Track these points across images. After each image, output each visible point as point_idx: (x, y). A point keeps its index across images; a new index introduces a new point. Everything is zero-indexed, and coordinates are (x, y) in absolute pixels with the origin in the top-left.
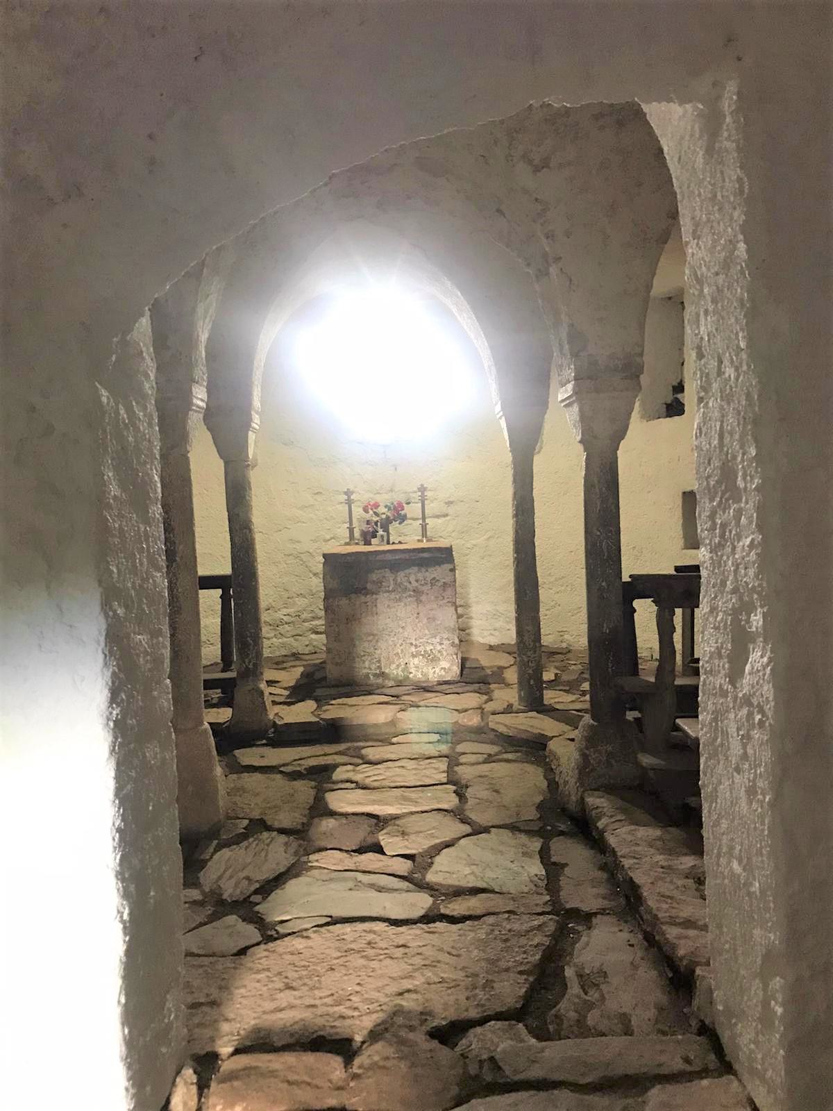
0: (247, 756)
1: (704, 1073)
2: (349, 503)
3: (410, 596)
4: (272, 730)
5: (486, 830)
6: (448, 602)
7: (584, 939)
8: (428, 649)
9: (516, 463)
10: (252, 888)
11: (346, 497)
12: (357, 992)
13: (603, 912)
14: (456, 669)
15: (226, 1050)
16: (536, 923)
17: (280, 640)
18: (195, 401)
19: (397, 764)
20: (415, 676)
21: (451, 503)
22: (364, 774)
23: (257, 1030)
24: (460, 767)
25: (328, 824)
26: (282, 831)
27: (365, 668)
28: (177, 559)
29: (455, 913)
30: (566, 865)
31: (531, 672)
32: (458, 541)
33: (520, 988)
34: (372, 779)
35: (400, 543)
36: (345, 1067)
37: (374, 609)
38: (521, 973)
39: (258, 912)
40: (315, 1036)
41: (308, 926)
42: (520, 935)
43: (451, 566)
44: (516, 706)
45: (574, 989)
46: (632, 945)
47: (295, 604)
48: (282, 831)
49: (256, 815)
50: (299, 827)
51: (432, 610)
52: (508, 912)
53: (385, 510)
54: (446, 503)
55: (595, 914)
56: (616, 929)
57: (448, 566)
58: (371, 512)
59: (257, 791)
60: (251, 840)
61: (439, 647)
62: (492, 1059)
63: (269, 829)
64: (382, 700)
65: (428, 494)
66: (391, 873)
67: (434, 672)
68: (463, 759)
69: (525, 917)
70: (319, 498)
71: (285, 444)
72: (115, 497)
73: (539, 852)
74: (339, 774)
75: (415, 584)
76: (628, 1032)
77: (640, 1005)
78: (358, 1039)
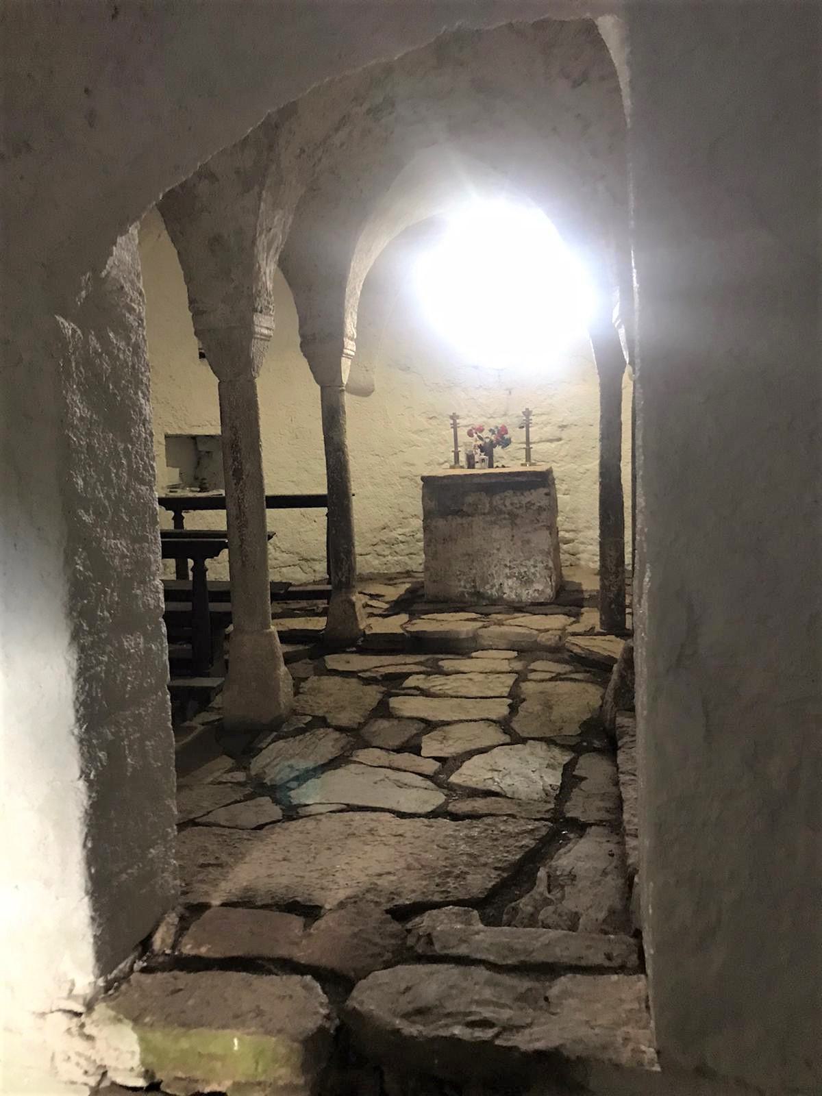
0: (334, 661)
1: (621, 969)
2: (455, 427)
3: (505, 519)
4: (362, 639)
5: (523, 741)
6: (544, 526)
7: (570, 845)
8: (522, 571)
9: (603, 387)
10: (292, 776)
11: (452, 422)
12: (343, 870)
13: (599, 823)
14: (549, 592)
15: (216, 902)
16: (530, 827)
17: (395, 558)
18: (257, 329)
19: (465, 676)
20: (509, 596)
21: (565, 426)
22: (437, 683)
23: (247, 889)
24: (528, 683)
25: (383, 724)
26: (339, 729)
27: (460, 586)
28: (244, 477)
29: (459, 812)
30: (585, 778)
31: (612, 596)
32: (569, 466)
33: (490, 882)
34: (439, 688)
35: (503, 467)
36: (305, 926)
37: (470, 530)
38: (496, 869)
39: (290, 797)
40: (291, 900)
41: (324, 811)
42: (511, 836)
43: (546, 490)
44: (598, 629)
45: (541, 887)
46: (612, 855)
47: (409, 523)
48: (339, 729)
49: (320, 713)
50: (355, 726)
51: (526, 533)
52: (509, 815)
53: (489, 435)
54: (560, 427)
55: (591, 825)
56: (604, 840)
57: (543, 491)
58: (475, 435)
59: (330, 692)
60: (308, 734)
61: (533, 570)
62: (429, 935)
63: (328, 726)
64: (470, 617)
65: (534, 419)
66: (420, 772)
67: (528, 594)
68: (532, 676)
69: (522, 821)
70: (434, 422)
71: (403, 370)
72: (82, 419)
73: (564, 766)
74: (411, 682)
75: (510, 507)
76: (573, 927)
77: (594, 907)
78: (327, 907)
